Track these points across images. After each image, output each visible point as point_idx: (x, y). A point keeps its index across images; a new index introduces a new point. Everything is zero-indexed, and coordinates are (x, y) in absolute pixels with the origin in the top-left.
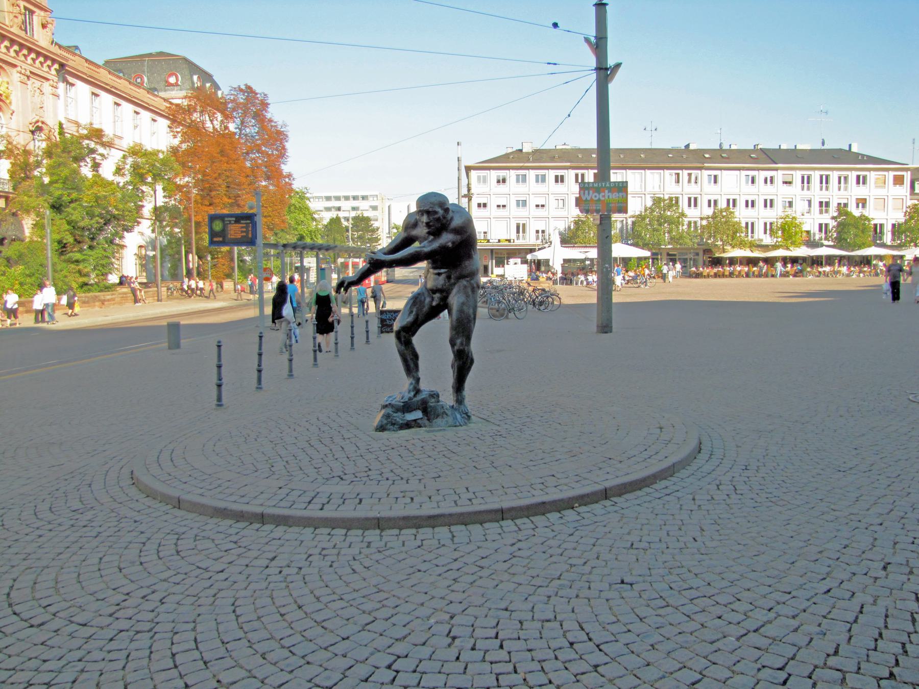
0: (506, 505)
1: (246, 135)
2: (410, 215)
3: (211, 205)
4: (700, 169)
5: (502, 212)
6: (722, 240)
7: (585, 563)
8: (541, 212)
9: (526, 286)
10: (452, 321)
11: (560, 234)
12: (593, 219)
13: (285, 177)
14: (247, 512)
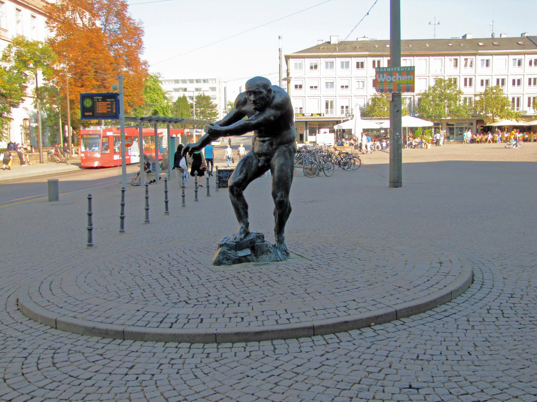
0: (317, 323)
1: (110, 30)
2: (241, 95)
3: (82, 86)
4: (475, 55)
5: (314, 92)
6: (492, 112)
7: (380, 371)
8: (345, 91)
9: (333, 150)
10: (274, 179)
11: (361, 109)
12: (386, 97)
13: (142, 64)
14: (111, 331)
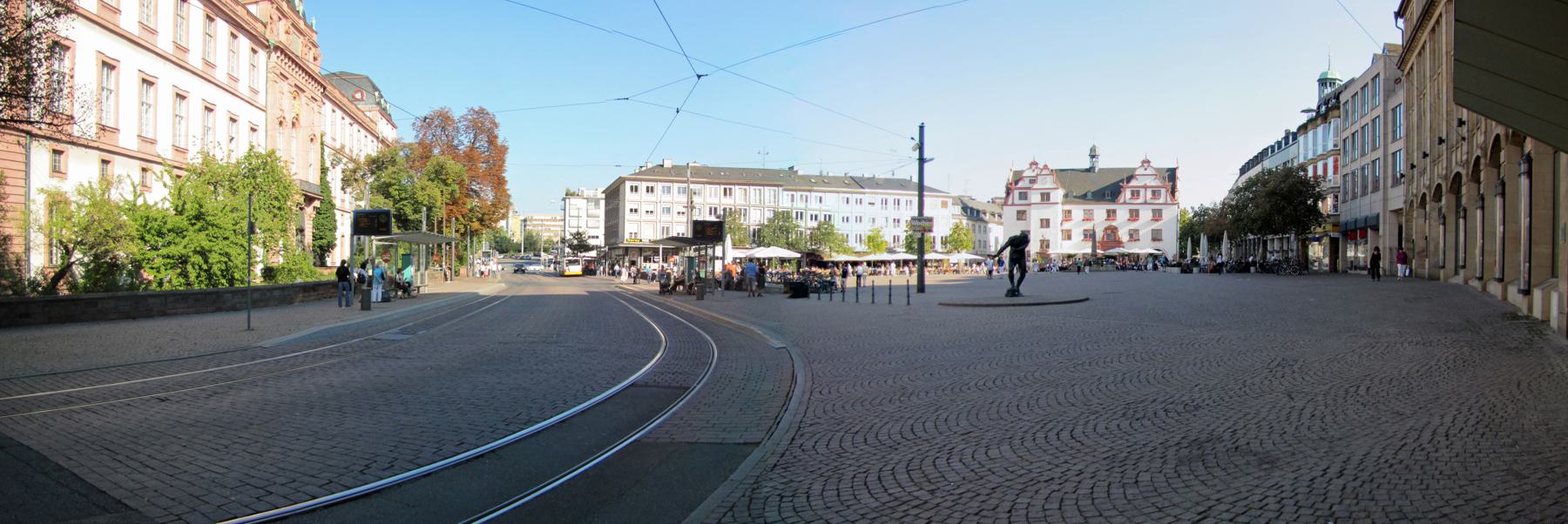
5: (650, 217)
